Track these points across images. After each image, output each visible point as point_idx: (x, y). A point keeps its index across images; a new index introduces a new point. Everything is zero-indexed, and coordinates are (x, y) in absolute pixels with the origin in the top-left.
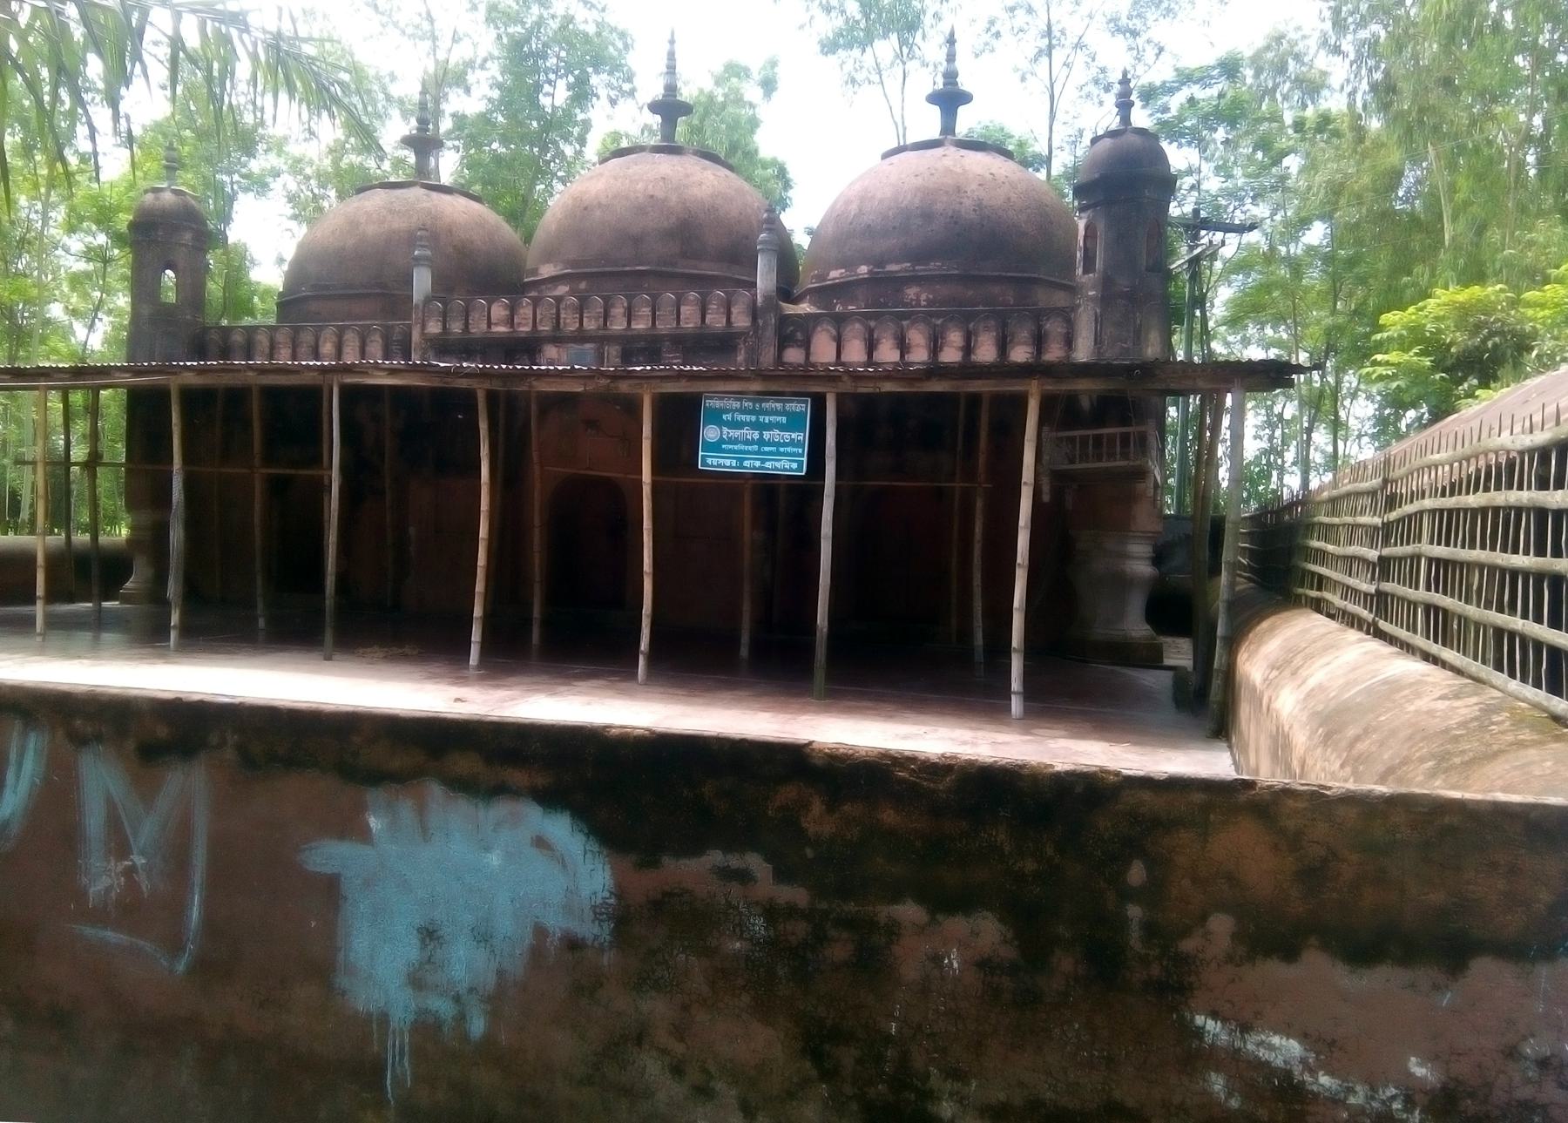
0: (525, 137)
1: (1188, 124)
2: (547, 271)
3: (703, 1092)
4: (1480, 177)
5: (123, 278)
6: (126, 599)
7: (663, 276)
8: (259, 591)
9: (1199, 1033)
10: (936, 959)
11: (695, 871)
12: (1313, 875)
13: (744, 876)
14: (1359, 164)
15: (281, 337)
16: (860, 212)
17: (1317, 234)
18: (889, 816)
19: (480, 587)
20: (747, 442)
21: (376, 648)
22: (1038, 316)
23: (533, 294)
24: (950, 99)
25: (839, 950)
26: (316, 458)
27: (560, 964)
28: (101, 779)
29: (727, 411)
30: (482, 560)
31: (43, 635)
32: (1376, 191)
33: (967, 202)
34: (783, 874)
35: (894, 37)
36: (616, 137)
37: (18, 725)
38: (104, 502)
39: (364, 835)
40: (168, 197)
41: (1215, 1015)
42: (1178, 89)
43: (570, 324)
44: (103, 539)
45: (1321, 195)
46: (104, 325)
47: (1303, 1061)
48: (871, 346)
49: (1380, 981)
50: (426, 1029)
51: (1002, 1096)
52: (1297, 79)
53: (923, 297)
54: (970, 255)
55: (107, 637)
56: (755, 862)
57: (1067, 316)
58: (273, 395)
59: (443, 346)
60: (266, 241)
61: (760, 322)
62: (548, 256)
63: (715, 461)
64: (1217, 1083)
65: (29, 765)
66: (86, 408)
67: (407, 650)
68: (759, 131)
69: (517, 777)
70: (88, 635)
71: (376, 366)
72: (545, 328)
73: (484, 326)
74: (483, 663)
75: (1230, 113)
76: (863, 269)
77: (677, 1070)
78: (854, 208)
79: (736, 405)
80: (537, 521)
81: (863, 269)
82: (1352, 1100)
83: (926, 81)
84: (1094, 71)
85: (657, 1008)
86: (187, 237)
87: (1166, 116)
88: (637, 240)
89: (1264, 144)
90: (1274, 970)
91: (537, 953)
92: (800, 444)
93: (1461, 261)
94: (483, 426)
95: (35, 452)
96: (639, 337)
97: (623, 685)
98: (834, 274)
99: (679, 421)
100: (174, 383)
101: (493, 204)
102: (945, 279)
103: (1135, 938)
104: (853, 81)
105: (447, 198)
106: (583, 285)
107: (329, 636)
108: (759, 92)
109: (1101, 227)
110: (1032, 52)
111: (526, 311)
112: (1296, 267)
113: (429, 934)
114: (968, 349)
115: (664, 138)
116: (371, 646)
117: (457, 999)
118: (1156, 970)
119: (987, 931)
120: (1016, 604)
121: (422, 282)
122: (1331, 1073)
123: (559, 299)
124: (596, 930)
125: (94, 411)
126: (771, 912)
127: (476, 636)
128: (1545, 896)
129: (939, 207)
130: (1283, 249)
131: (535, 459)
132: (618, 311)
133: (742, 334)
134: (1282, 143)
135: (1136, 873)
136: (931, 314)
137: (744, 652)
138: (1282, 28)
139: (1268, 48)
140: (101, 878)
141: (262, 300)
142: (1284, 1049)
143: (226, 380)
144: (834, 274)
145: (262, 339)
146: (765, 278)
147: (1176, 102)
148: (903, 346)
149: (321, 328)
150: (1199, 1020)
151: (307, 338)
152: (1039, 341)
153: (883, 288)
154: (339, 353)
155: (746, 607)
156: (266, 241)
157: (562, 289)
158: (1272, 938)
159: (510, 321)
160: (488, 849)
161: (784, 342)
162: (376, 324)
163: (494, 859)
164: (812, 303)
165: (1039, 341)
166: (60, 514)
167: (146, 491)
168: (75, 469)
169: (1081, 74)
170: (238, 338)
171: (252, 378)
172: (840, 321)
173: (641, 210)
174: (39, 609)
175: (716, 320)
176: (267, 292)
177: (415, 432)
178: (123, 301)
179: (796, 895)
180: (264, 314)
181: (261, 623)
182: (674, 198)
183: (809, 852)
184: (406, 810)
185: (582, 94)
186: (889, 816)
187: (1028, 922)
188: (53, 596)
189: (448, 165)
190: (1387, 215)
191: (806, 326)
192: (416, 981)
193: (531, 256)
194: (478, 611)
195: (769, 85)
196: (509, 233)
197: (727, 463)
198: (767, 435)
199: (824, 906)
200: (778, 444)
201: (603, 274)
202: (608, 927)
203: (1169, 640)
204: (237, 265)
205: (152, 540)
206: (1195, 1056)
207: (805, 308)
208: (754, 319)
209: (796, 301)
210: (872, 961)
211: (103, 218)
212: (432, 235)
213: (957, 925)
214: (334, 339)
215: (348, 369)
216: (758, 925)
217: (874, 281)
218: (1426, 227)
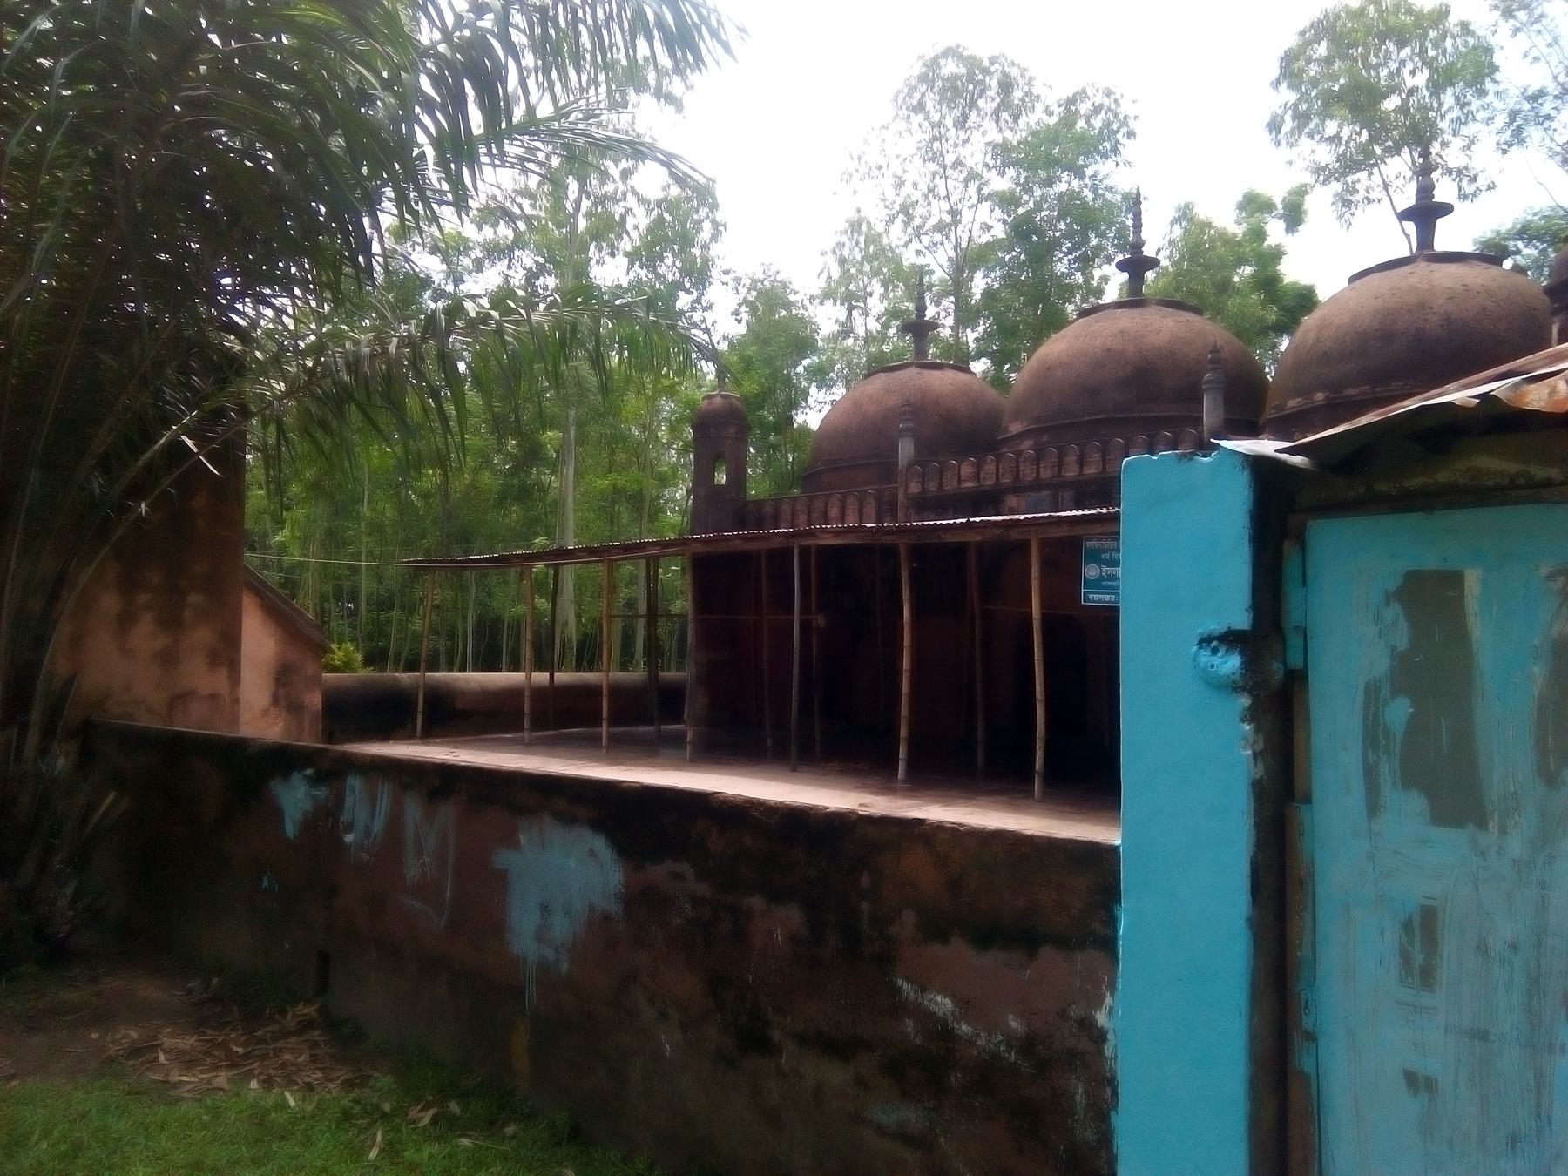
2: (1015, 428)
3: (663, 1016)
9: (899, 990)
11: (659, 872)
13: (679, 876)
19: (904, 711)
29: (1105, 551)
40: (718, 400)
41: (907, 979)
43: (1028, 474)
49: (992, 960)
50: (543, 967)
56: (686, 868)
59: (924, 505)
62: (1017, 416)
72: (1006, 480)
73: (955, 483)
74: (906, 781)
81: (1320, 396)
86: (732, 430)
98: (1292, 403)
105: (937, 373)
106: (1045, 438)
108: (1281, 224)
111: (990, 466)
113: (545, 909)
121: (906, 450)
122: (967, 1023)
127: (902, 753)
132: (1071, 459)
135: (865, 881)
140: (412, 869)
142: (943, 1004)
149: (845, 496)
158: (936, 929)
163: (572, 863)
174: (604, 729)
179: (703, 889)
192: (540, 937)
194: (903, 733)
197: (1107, 597)
206: (899, 1008)
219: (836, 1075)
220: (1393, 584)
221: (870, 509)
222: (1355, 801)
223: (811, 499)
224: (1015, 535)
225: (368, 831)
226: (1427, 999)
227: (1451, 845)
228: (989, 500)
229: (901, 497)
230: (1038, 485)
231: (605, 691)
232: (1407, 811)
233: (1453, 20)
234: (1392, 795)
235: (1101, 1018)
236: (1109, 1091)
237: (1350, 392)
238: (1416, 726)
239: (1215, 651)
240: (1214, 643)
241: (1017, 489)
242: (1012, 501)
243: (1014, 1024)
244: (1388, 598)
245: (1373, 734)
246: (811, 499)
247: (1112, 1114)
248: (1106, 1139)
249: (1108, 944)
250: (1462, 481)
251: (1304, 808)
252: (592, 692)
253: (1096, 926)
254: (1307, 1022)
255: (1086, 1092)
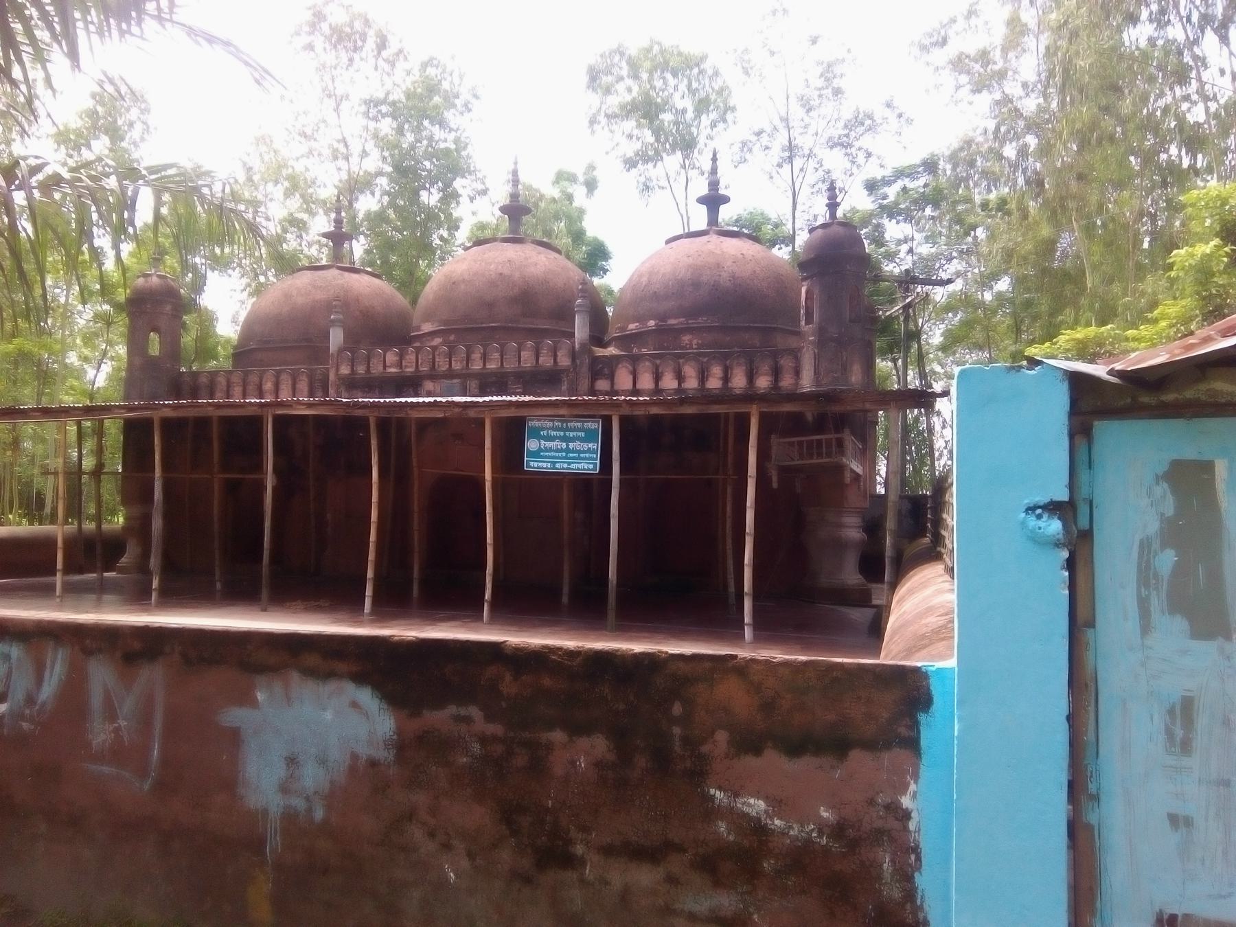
0: (410, 235)
1: (903, 206)
2: (427, 327)
3: (447, 847)
4: (1109, 244)
5: (122, 335)
6: (121, 570)
7: (508, 330)
8: (217, 563)
10: (573, 763)
11: (440, 718)
12: (768, 707)
13: (467, 720)
14: (1023, 235)
15: (236, 379)
16: (649, 283)
17: (1003, 285)
18: (547, 682)
19: (371, 556)
20: (558, 451)
21: (299, 602)
22: (775, 355)
23: (417, 344)
24: (713, 201)
25: (521, 760)
26: (259, 467)
27: (366, 775)
28: (101, 675)
29: (543, 429)
30: (373, 537)
31: (61, 597)
32: (1036, 254)
33: (724, 275)
34: (489, 718)
35: (679, 154)
36: (482, 227)
37: (52, 643)
38: (106, 497)
39: (254, 703)
41: (720, 788)
42: (895, 181)
43: (443, 366)
44: (105, 526)
45: (999, 258)
46: (107, 368)
47: (766, 812)
48: (657, 378)
49: (805, 764)
50: (289, 817)
51: (609, 840)
52: (983, 172)
53: (695, 342)
54: (721, 313)
55: (108, 598)
56: (474, 712)
57: (795, 354)
58: (228, 422)
59: (352, 384)
60: (227, 304)
61: (578, 362)
62: (428, 317)
63: (536, 464)
64: (722, 827)
65: (58, 668)
66: (94, 431)
67: (321, 603)
68: (585, 217)
69: (341, 667)
70: (94, 596)
71: (299, 402)
72: (424, 369)
73: (381, 368)
74: (371, 614)
75: (934, 198)
76: (652, 323)
77: (432, 835)
78: (645, 279)
79: (550, 424)
80: (416, 508)
81: (652, 323)
82: (792, 833)
83: (701, 187)
84: (821, 173)
85: (420, 799)
86: (168, 308)
87: (885, 202)
88: (490, 305)
89: (958, 220)
90: (750, 761)
91: (352, 770)
92: (595, 452)
93: (1097, 305)
94: (374, 443)
95: (57, 463)
96: (493, 373)
97: (473, 624)
98: (632, 326)
99: (512, 433)
100: (156, 416)
101: (391, 279)
102: (709, 329)
103: (677, 747)
104: (647, 187)
106: (452, 338)
107: (265, 593)
108: (584, 190)
109: (816, 292)
110: (776, 160)
111: (411, 357)
112: (990, 311)
113: (292, 761)
114: (726, 379)
115: (512, 232)
116: (295, 600)
117: (308, 799)
118: (688, 764)
119: (599, 745)
120: (746, 561)
121: (336, 338)
123: (434, 348)
124: (386, 754)
125: (100, 433)
126: (484, 740)
127: (369, 592)
128: (886, 715)
129: (704, 279)
130: (988, 296)
131: (415, 464)
132: (477, 356)
133: (565, 371)
134: (971, 219)
135: (677, 709)
136: (700, 354)
137: (565, 599)
138: (971, 134)
139: (962, 149)
140: (100, 734)
141: (224, 348)
142: (756, 806)
143: (191, 413)
144: (632, 326)
145: (222, 380)
146: (581, 330)
147: (892, 192)
148: (680, 378)
150: (712, 791)
151: (254, 379)
152: (776, 373)
153: (665, 335)
154: (277, 391)
155: (566, 568)
156: (227, 304)
157: (437, 341)
158: (749, 743)
159: (400, 365)
160: (324, 709)
161: (595, 375)
162: (303, 368)
163: (328, 715)
164: (617, 347)
165: (776, 373)
166: (74, 509)
167: (136, 491)
168: (85, 478)
169: (811, 177)
170: (203, 380)
171: (211, 412)
172: (635, 360)
173: (492, 284)
174: (59, 579)
175: (546, 361)
176: (228, 341)
177: (325, 446)
178: (122, 350)
179: (495, 729)
180: (222, 361)
181: (219, 586)
182: (517, 274)
183: (504, 704)
184: (278, 687)
185: (450, 196)
186: (547, 682)
187: (620, 737)
188: (68, 570)
189: (359, 248)
190: (1044, 272)
191: (613, 362)
192: (284, 789)
193: (417, 315)
194: (370, 574)
195: (591, 185)
196: (401, 300)
197: (545, 465)
198: (571, 445)
199: (512, 734)
200: (580, 452)
201: (466, 330)
202: (393, 752)
203: (874, 585)
204: (207, 320)
205: (139, 527)
206: (711, 813)
207: (612, 351)
208: (574, 360)
209: (603, 345)
210: (538, 766)
211: (106, 290)
212: (344, 304)
213: (583, 742)
214: (273, 379)
215: (281, 404)
216: (476, 748)
217: (660, 331)
218: (1073, 278)
219: (645, 877)
220: (1162, 468)
221: (303, 385)
222: (1132, 624)
223: (246, 373)
224: (472, 413)
225: (30, 700)
226: (1186, 761)
227: (1207, 650)
228: (411, 384)
229: (332, 377)
230: (450, 374)
231: (60, 543)
232: (1171, 631)
233: (706, 65)
234: (1160, 618)
235: (906, 802)
236: (913, 857)
237: (672, 322)
238: (1179, 571)
239: (1039, 517)
240: (1039, 511)
241: (433, 376)
242: (429, 385)
243: (825, 815)
244: (1158, 479)
245: (1146, 575)
246: (246, 373)
247: (916, 875)
248: (910, 894)
249: (912, 744)
250: (1203, 398)
251: (1090, 632)
252: (47, 544)
253: (903, 731)
254: (1092, 788)
255: (893, 861)
